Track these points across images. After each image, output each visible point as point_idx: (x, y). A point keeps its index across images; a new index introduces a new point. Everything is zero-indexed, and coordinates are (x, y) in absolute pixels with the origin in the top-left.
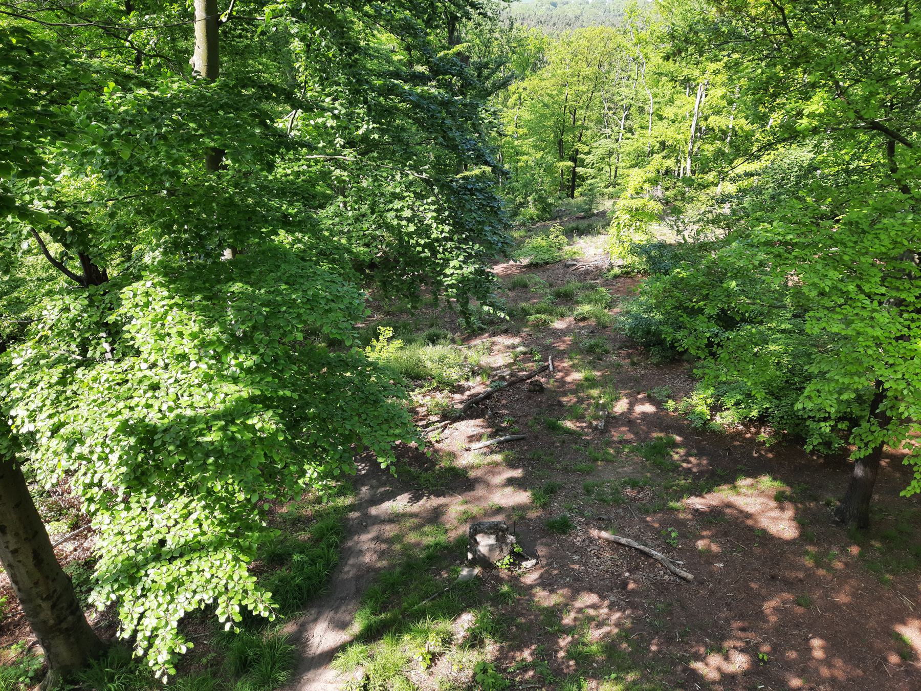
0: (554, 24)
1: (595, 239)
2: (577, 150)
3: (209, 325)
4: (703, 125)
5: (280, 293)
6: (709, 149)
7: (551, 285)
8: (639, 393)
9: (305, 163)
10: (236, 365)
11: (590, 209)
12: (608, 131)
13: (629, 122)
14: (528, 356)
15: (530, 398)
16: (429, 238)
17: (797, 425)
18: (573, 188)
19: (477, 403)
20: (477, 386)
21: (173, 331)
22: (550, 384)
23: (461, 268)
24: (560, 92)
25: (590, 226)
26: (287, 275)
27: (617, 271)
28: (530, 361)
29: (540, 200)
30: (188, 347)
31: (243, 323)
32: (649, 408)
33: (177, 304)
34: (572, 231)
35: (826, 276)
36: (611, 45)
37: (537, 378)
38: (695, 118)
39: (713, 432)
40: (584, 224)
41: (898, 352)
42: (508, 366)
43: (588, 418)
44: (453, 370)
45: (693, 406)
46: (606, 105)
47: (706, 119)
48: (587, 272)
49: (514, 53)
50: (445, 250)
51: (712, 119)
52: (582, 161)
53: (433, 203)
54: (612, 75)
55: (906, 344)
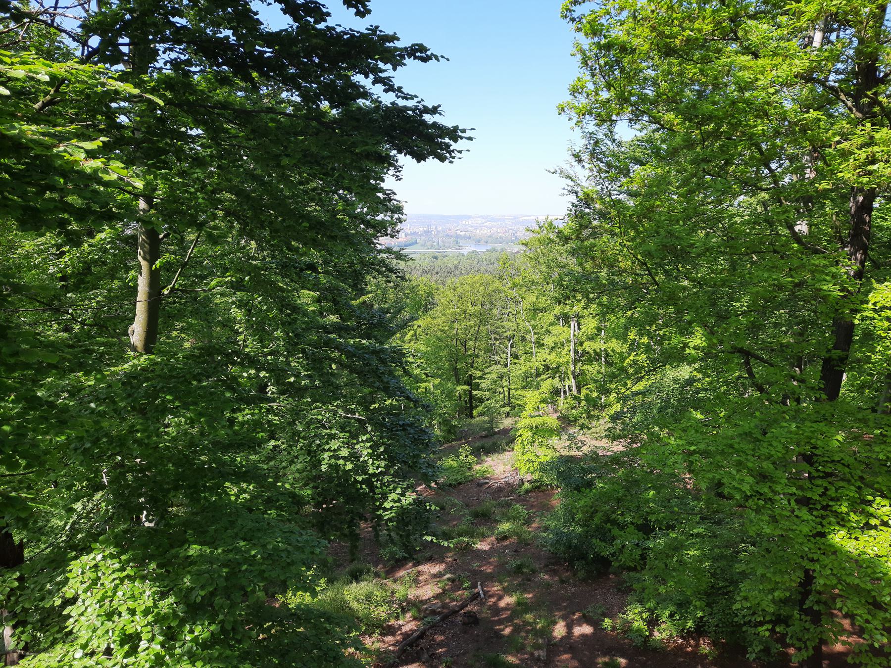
0: (437, 273)
1: (501, 456)
2: (471, 375)
3: (163, 595)
4: (580, 349)
5: (238, 550)
6: (592, 370)
7: (467, 506)
8: (574, 614)
9: (250, 412)
10: (192, 641)
11: (492, 428)
12: (497, 358)
13: (514, 349)
14: (456, 583)
15: (465, 632)
16: (366, 473)
17: (733, 632)
18: (472, 408)
19: (411, 645)
20: (408, 624)
21: (123, 609)
22: (485, 613)
23: (399, 500)
24: (451, 328)
25: (495, 444)
26: (245, 530)
27: (527, 485)
28: (459, 589)
29: (445, 422)
30: (139, 624)
31: (203, 588)
32: (587, 629)
33: (128, 576)
34: (479, 450)
35: (743, 480)
36: (490, 289)
37: (470, 608)
38: (572, 344)
39: (655, 650)
40: (488, 443)
41: (820, 549)
42: (437, 596)
43: (529, 649)
44: (381, 609)
45: (629, 623)
46: (493, 336)
47: (581, 344)
48: (500, 489)
49: (408, 298)
50: (383, 484)
51: (586, 344)
52: (478, 385)
53: (367, 441)
54: (495, 312)
55: (823, 540)
